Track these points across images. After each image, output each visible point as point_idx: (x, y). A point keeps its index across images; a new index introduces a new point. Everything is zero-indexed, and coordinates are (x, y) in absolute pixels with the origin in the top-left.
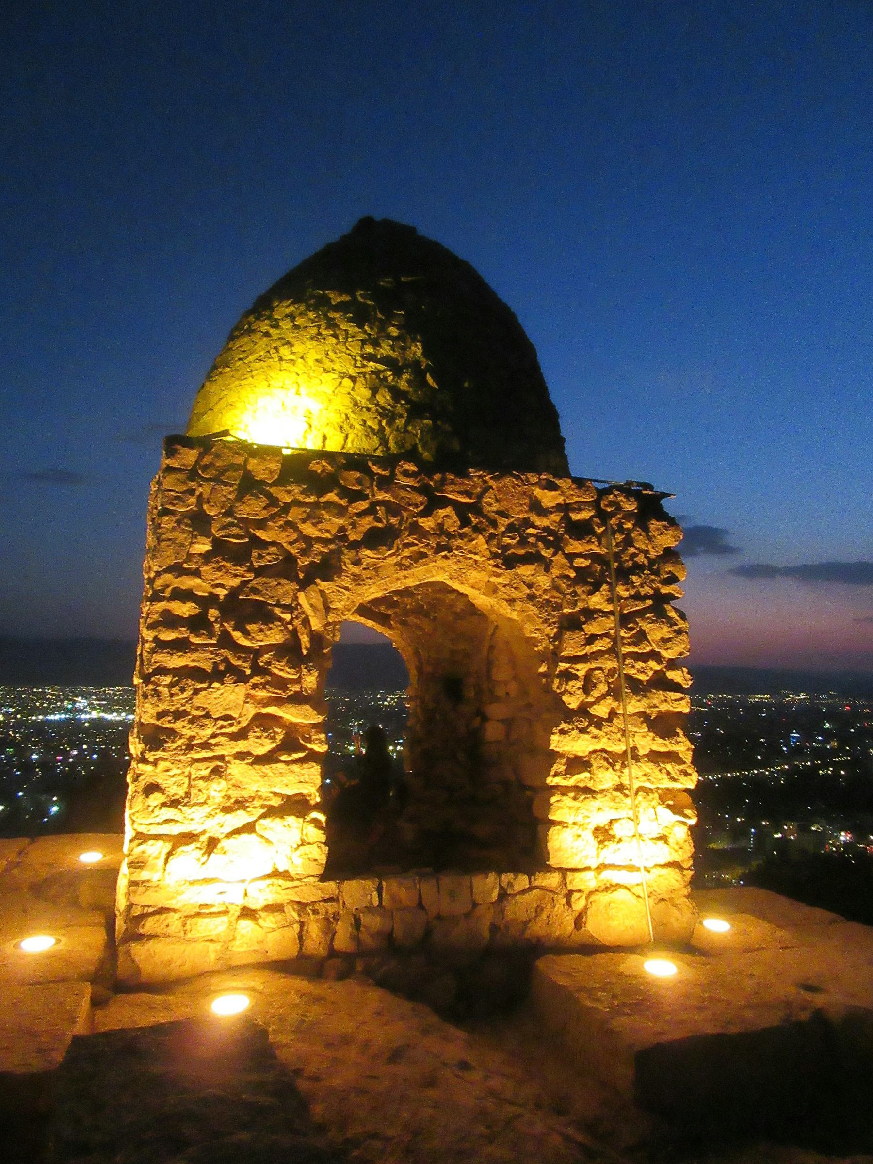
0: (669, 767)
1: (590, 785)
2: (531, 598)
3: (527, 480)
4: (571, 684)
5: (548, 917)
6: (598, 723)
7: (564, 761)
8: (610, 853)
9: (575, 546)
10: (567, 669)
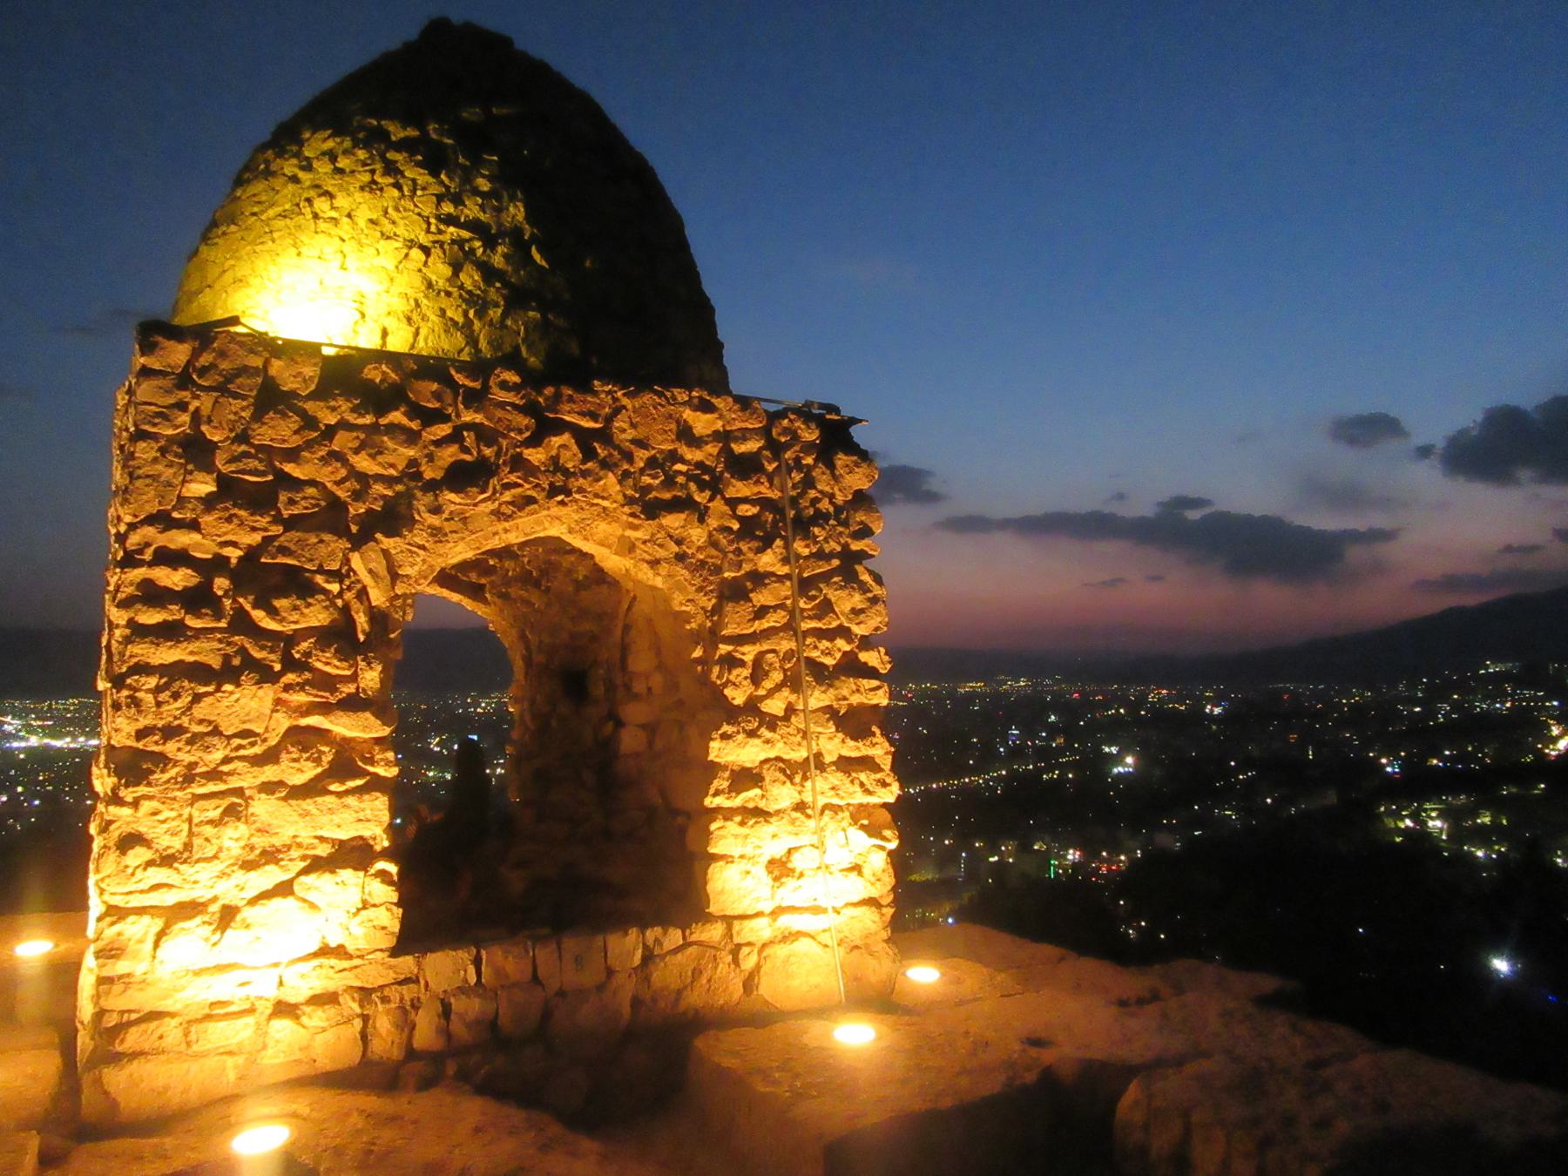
0: (863, 777)
1: (762, 804)
2: (681, 558)
4: (735, 672)
8: (789, 893)
9: (739, 489)
10: (729, 653)
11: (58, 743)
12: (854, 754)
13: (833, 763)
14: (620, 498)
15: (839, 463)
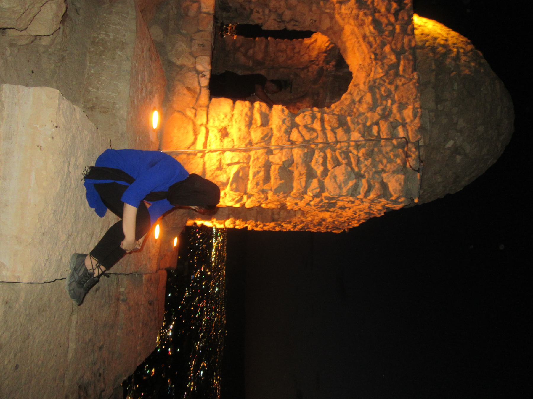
0: (262, 174)
1: (254, 126)
2: (353, 102)
3: (416, 102)
4: (309, 118)
5: (184, 94)
6: (288, 132)
7: (267, 112)
8: (214, 134)
9: (384, 126)
10: (316, 117)
11: (214, 250)
12: (271, 172)
13: (268, 160)
14: (375, 78)
15: (400, 176)
